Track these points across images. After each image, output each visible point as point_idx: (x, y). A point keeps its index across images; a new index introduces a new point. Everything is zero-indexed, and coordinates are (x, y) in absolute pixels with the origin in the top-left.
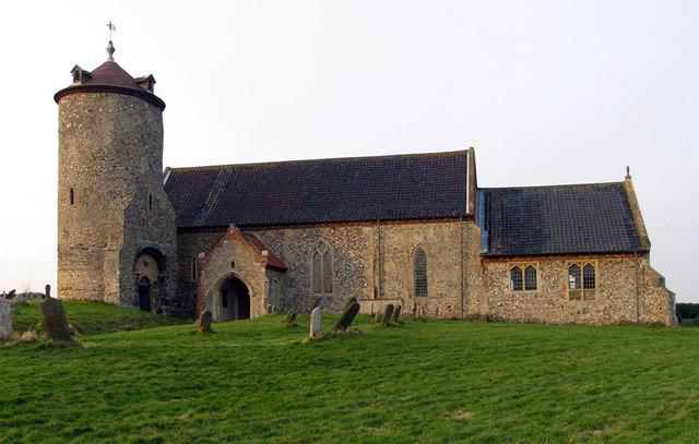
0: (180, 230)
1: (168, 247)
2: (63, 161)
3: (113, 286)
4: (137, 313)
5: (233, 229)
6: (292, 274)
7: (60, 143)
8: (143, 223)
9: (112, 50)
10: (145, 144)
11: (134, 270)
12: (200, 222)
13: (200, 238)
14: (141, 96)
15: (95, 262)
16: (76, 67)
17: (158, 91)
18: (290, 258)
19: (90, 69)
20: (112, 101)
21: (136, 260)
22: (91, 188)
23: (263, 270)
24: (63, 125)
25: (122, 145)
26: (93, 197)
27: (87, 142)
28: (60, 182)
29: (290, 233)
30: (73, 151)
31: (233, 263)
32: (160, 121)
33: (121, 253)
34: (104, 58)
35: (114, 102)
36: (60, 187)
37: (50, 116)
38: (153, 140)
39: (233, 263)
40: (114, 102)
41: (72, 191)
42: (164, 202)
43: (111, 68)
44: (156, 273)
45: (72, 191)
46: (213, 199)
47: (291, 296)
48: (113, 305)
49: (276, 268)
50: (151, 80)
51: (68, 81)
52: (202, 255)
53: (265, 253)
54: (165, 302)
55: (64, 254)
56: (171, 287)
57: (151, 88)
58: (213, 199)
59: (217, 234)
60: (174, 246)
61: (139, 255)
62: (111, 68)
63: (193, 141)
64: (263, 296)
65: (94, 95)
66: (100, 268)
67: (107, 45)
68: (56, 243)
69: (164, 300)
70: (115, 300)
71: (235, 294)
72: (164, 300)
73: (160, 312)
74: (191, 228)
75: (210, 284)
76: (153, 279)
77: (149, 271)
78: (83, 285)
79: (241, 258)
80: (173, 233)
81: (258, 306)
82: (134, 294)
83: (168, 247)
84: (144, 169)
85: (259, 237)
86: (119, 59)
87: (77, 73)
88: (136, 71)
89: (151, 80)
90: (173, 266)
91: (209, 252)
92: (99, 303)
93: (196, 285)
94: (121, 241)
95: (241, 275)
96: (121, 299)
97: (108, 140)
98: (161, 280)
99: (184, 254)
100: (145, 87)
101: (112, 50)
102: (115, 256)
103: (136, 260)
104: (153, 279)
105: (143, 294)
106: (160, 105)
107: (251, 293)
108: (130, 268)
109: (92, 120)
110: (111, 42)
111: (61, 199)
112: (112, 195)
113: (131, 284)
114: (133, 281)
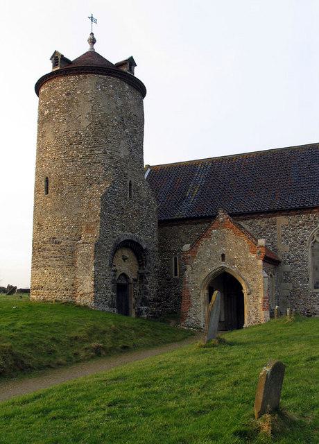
0: (162, 223)
1: (149, 239)
2: (41, 149)
3: (87, 285)
4: (111, 320)
5: (222, 216)
6: (287, 267)
7: (39, 132)
8: (122, 212)
9: (93, 41)
10: (124, 127)
11: (111, 265)
12: (182, 214)
13: (182, 230)
14: (122, 79)
15: (68, 258)
16: (55, 52)
17: (138, 73)
18: (284, 249)
19: (72, 59)
20: (89, 83)
21: (113, 255)
22: (66, 175)
23: (260, 263)
24: (41, 113)
25: (99, 126)
26: (67, 184)
27: (63, 127)
28: (37, 173)
29: (282, 220)
30: (50, 137)
31: (223, 256)
32: (141, 105)
33: (97, 245)
34: (86, 48)
35: (94, 92)
36: (36, 178)
37: (31, 104)
38: (133, 125)
39: (223, 256)
40: (94, 92)
41: (47, 181)
42: (145, 192)
43: (92, 54)
44: (136, 268)
45: (47, 181)
46: (194, 191)
47: (286, 293)
48: (85, 307)
49: (271, 261)
50: (131, 63)
51: (48, 68)
52: (186, 247)
53: (262, 242)
54: (145, 302)
55: (37, 249)
56: (152, 285)
57: (131, 70)
58: (194, 191)
59: (200, 226)
60: (156, 239)
61: (116, 250)
62: (92, 54)
63: (168, 141)
64: (261, 294)
65: (72, 78)
66: (73, 263)
67: (88, 36)
68: (31, 238)
69: (144, 299)
70: (88, 301)
71: (228, 287)
72: (144, 299)
73: (139, 314)
74: (173, 221)
75: (197, 276)
76: (132, 276)
77: (127, 266)
78: (55, 287)
79: (236, 250)
80: (154, 224)
81: (255, 309)
82: (110, 294)
83: (149, 239)
84: (124, 153)
85: (246, 227)
86: (98, 48)
87: (57, 59)
88: (114, 58)
89: (131, 63)
90: (154, 261)
91: (195, 244)
92: (70, 306)
93: (180, 281)
94: (97, 233)
95: (234, 270)
96: (95, 300)
97: (85, 123)
98: (141, 276)
99: (164, 248)
100: (125, 69)
101: (93, 41)
102: (89, 249)
103: (113, 255)
104: (132, 276)
105: (120, 294)
106: (140, 89)
107: (245, 291)
108: (106, 263)
109: (69, 102)
110: (92, 34)
111: (37, 191)
112: (90, 182)
113: (107, 283)
114: (109, 279)
